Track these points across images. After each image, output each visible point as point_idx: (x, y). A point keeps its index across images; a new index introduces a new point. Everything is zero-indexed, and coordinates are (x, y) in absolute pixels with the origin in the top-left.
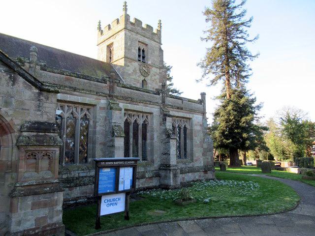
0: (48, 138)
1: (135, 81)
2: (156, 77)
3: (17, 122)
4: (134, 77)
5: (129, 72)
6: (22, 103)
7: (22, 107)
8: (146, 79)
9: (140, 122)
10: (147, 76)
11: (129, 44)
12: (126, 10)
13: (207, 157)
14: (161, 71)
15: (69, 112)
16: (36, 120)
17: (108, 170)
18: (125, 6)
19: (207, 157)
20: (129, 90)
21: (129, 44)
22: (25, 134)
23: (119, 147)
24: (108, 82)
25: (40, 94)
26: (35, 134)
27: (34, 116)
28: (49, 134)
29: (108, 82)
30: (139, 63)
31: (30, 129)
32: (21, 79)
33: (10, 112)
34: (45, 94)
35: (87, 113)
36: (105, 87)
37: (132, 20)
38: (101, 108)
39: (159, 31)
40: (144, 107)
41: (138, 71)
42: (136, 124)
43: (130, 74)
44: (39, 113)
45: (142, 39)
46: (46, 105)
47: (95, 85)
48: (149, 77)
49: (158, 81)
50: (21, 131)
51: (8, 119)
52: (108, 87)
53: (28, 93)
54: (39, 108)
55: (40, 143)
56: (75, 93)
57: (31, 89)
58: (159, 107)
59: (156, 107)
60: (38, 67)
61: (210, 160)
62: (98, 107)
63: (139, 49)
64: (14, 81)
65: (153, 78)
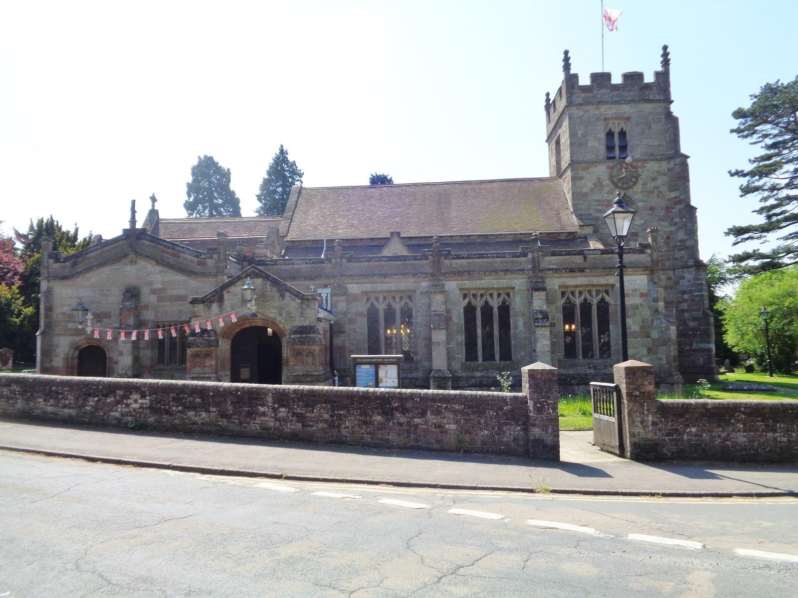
0: (309, 339)
1: (598, 205)
2: (658, 182)
3: (288, 327)
4: (597, 196)
5: (584, 190)
6: (289, 313)
7: (290, 317)
8: (630, 193)
9: (495, 303)
10: (632, 187)
11: (580, 133)
12: (567, 66)
13: (659, 356)
14: (672, 165)
15: (384, 304)
16: (301, 324)
17: (367, 367)
18: (567, 59)
19: (659, 356)
20: (465, 261)
21: (580, 133)
22: (293, 336)
23: (439, 343)
24: (430, 258)
25: (302, 303)
26: (299, 336)
27: (299, 322)
28: (310, 335)
29: (430, 258)
30: (610, 163)
31: (295, 333)
32: (288, 294)
33: (283, 321)
34: (306, 302)
35: (408, 301)
36: (426, 264)
37: (585, 80)
38: (421, 293)
39: (663, 77)
40: (495, 281)
41: (606, 182)
42: (487, 310)
43: (586, 195)
44: (303, 319)
46: (308, 311)
47: (411, 265)
48: (638, 187)
49: (664, 189)
50: (290, 335)
51: (281, 326)
52: (432, 264)
53: (293, 304)
54: (302, 314)
55: (302, 342)
56: (387, 280)
57: (295, 300)
58: (526, 276)
59: (521, 276)
60: (344, 260)
61: (664, 362)
62: (418, 293)
63: (610, 134)
64: (283, 296)
65: (651, 185)
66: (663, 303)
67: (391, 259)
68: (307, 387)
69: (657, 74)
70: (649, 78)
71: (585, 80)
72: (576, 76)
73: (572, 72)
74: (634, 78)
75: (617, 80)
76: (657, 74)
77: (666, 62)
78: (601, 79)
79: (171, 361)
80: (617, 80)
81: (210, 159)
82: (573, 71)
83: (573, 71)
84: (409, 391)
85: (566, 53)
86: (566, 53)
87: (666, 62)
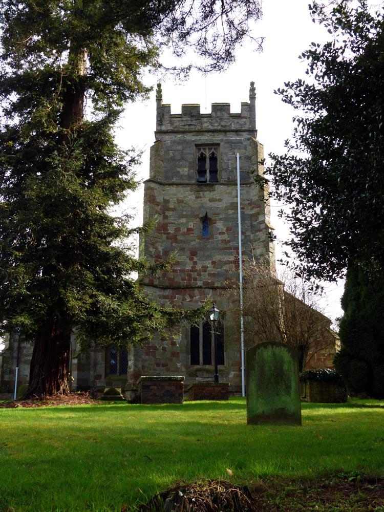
37: (176, 110)
39: (249, 108)
45: (205, 138)
66: (174, 358)
67: (20, 410)
68: (242, 345)
69: (244, 105)
70: (236, 109)
71: (176, 110)
72: (168, 107)
73: (164, 102)
74: (221, 109)
75: (206, 109)
76: (244, 105)
77: (253, 97)
78: (191, 111)
79: (207, 361)
80: (206, 109)
81: (229, 106)
82: (164, 102)
83: (164, 102)
84: (243, 348)
85: (252, 84)
86: (252, 84)
87: (253, 97)
